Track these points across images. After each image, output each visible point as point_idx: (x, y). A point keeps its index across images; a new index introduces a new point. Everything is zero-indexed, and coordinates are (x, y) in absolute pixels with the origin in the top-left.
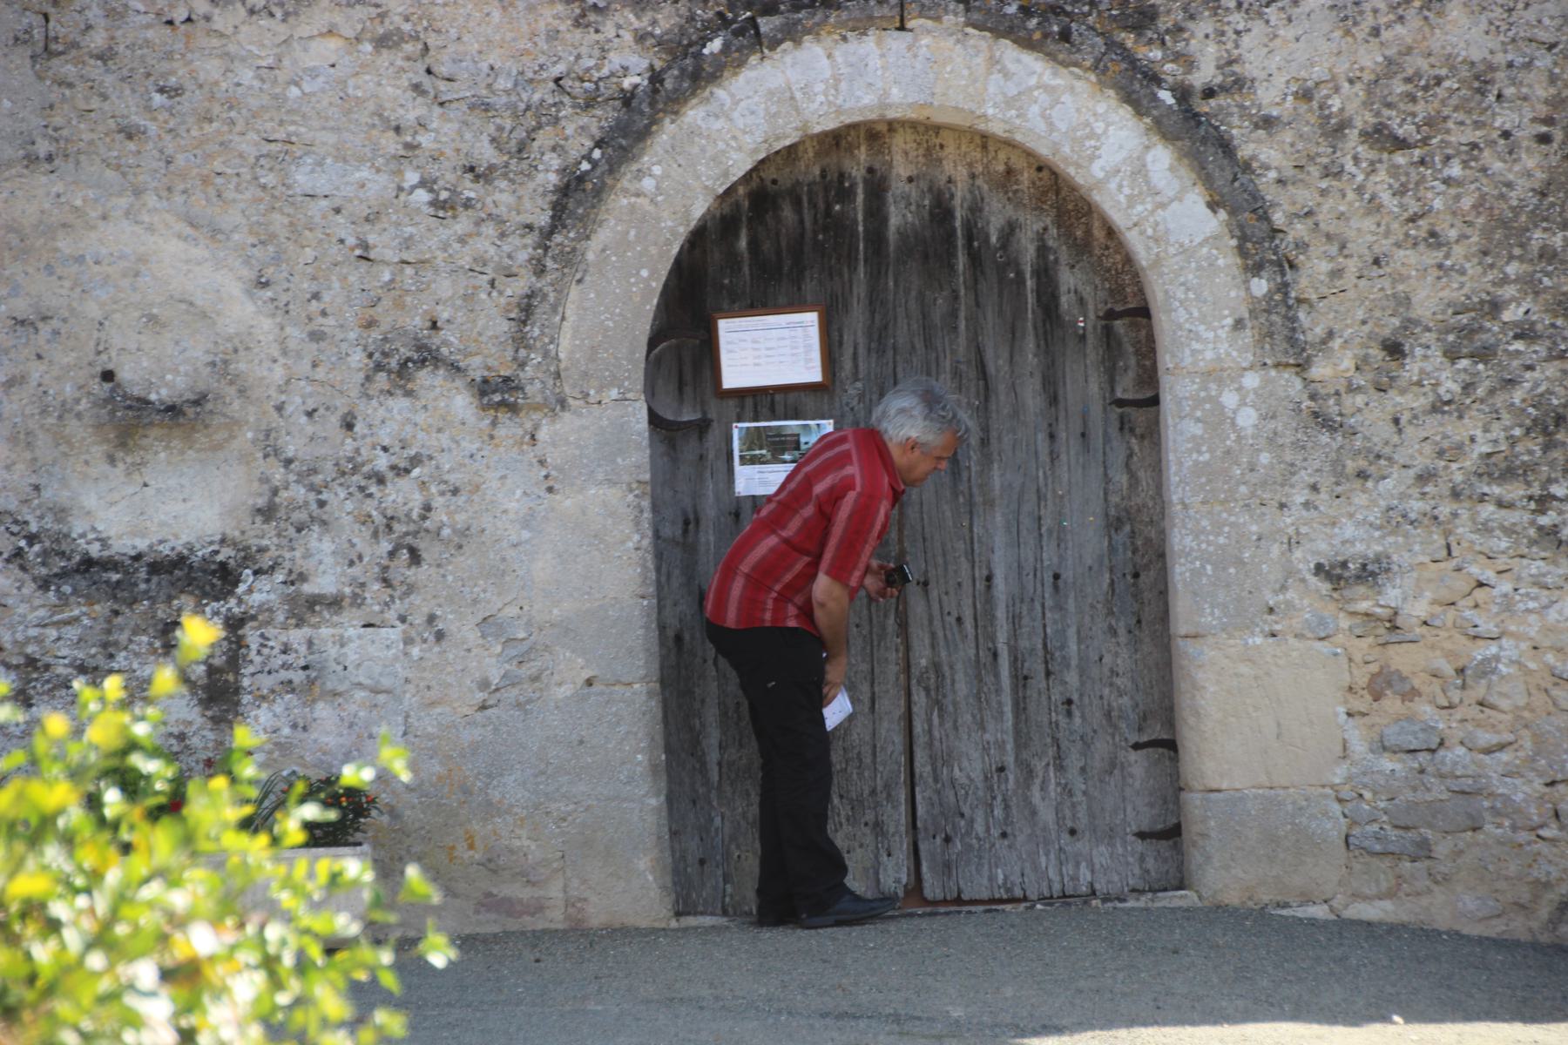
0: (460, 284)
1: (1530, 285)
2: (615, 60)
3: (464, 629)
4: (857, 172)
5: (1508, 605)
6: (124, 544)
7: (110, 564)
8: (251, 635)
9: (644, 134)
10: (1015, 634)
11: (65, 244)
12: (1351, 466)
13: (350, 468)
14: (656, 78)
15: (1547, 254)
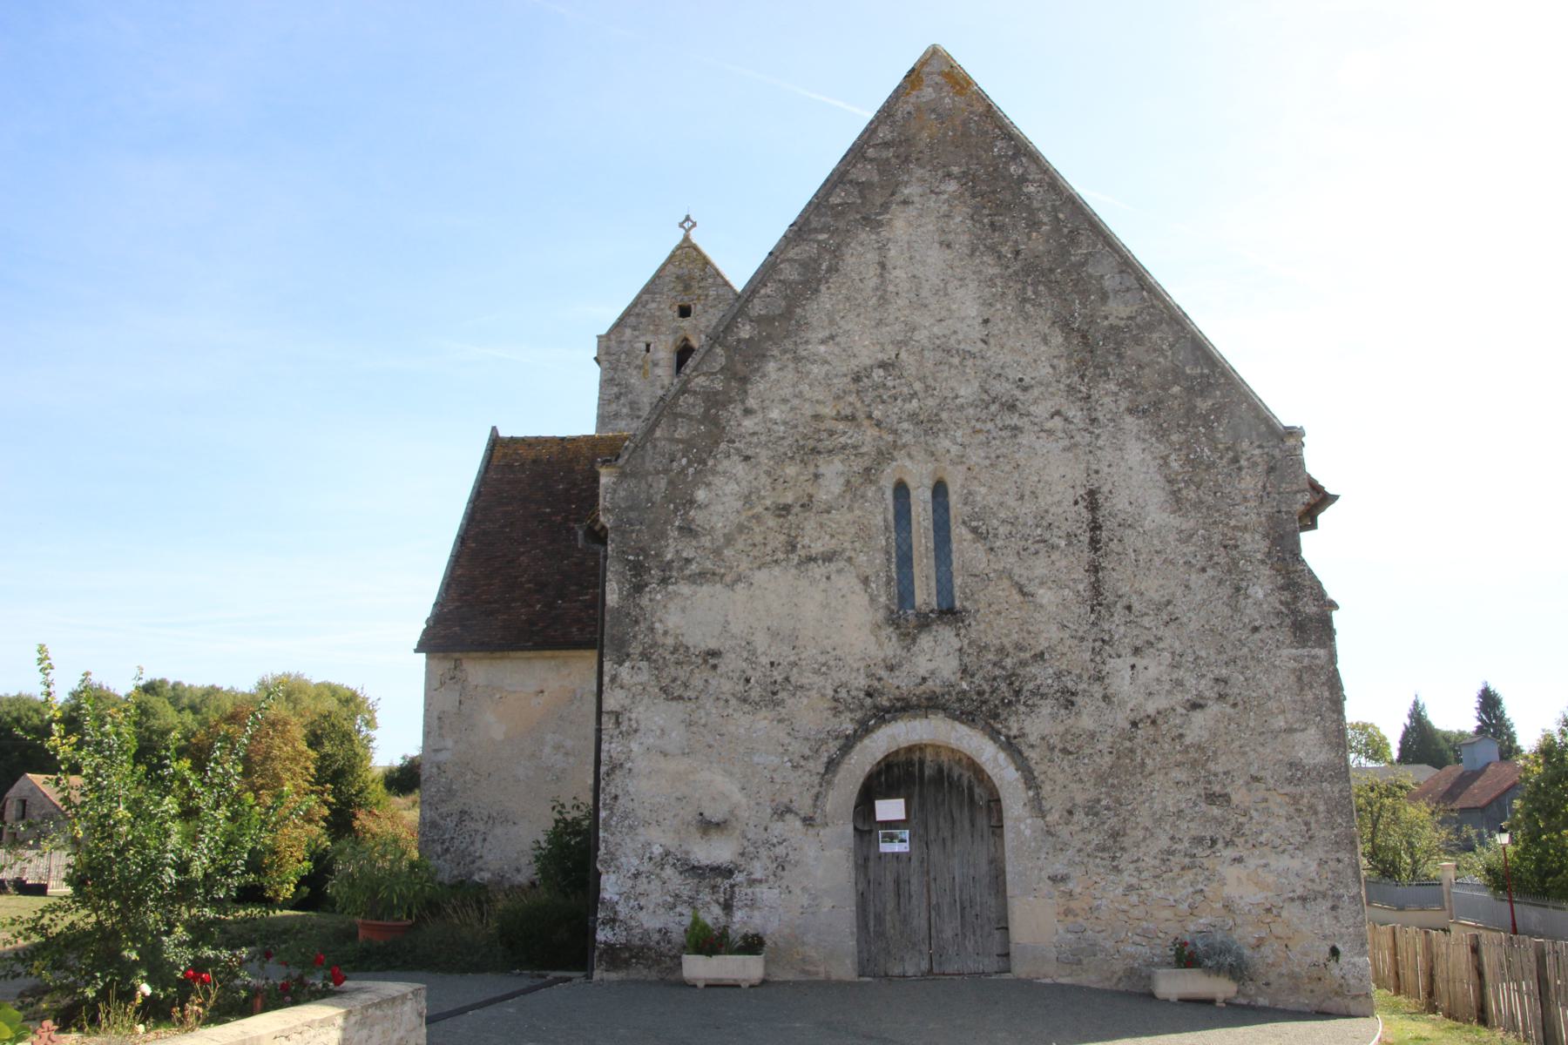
1: (1108, 794)
3: (797, 891)
5: (1104, 889)
6: (705, 862)
8: (737, 889)
9: (852, 747)
11: (691, 777)
15: (1113, 786)
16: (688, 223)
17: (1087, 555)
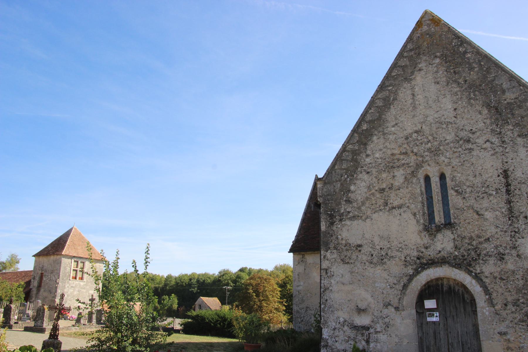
0: (393, 297)
1: (523, 297)
2: (409, 271)
4: (440, 283)
5: (525, 339)
6: (359, 324)
7: (357, 327)
10: (461, 339)
11: (353, 292)
12: (501, 320)
13: (381, 317)
14: (413, 273)
15: (525, 293)
17: (505, 197)
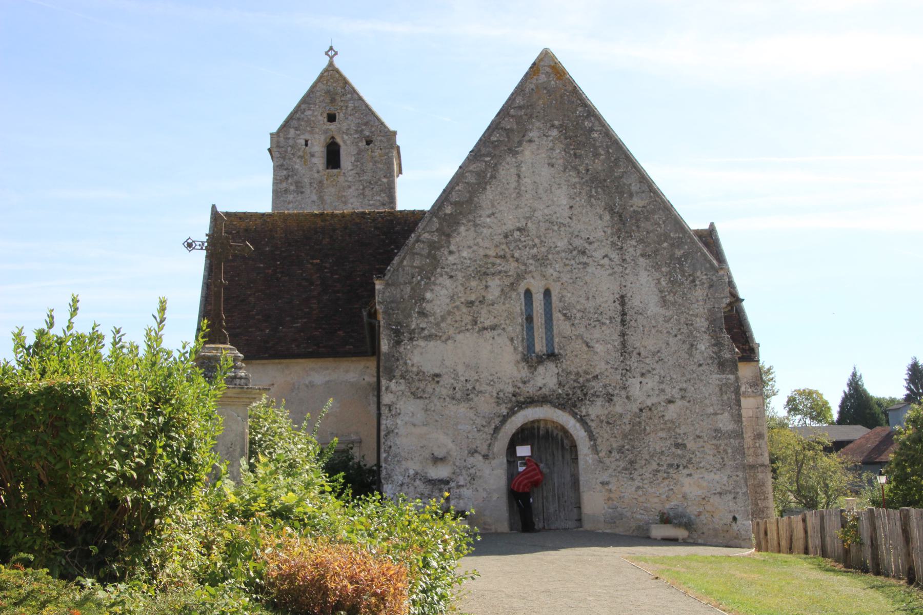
16: (331, 52)
